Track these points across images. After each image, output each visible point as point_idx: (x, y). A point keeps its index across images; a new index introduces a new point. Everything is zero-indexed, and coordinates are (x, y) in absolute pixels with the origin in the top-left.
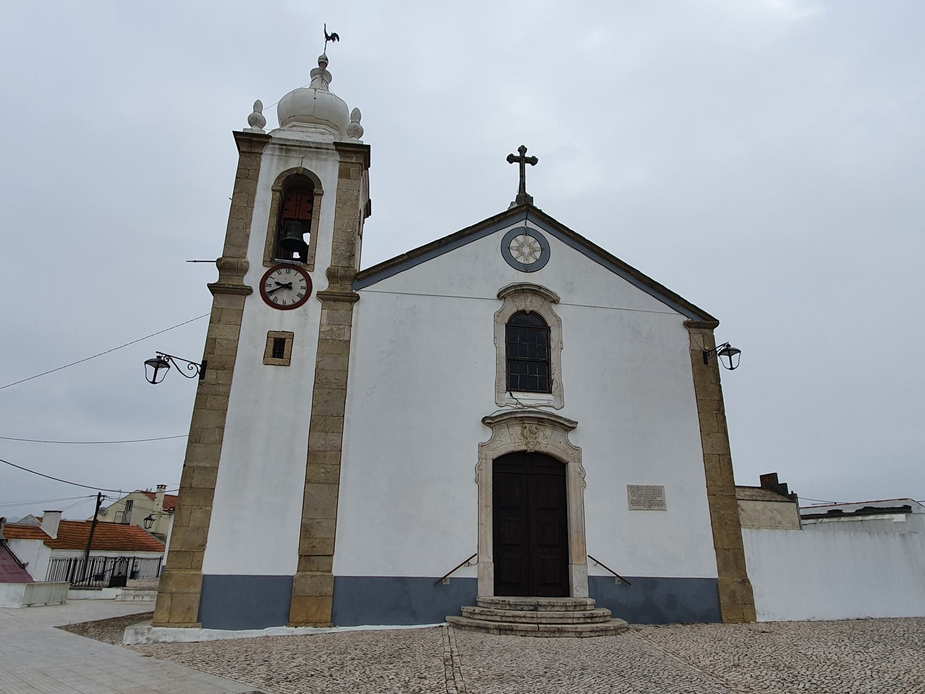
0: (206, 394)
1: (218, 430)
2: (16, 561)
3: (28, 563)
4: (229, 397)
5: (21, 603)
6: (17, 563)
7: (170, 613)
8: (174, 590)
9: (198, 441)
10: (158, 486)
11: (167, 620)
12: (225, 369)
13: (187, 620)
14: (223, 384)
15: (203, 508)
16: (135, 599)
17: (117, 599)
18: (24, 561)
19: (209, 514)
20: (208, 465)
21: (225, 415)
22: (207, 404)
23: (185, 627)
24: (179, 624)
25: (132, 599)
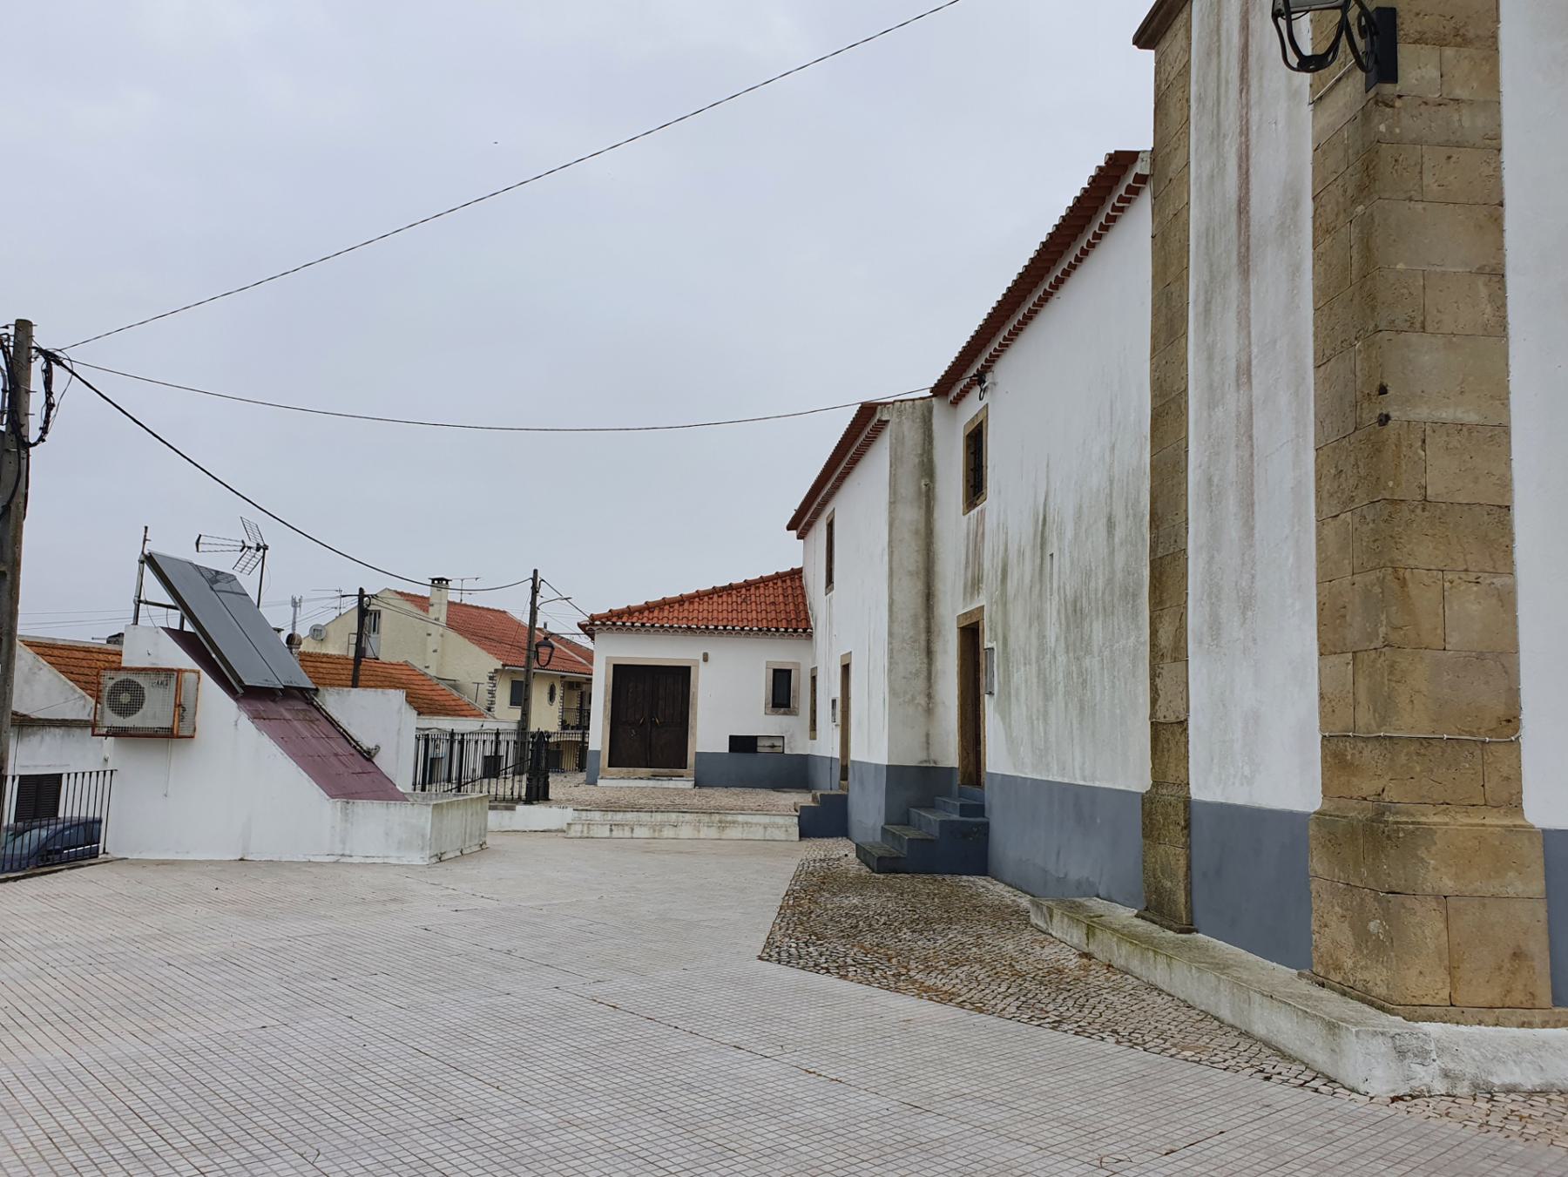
0: (1414, 142)
1: (1486, 285)
2: (350, 744)
3: (377, 748)
4: (1500, 150)
5: (428, 852)
6: (354, 747)
7: (1452, 970)
8: (1448, 884)
9: (1418, 325)
10: (433, 580)
11: (1445, 993)
12: (1466, 42)
13: (1518, 997)
14: (1472, 102)
15: (1486, 579)
16: (615, 834)
17: (572, 833)
18: (367, 743)
19: (1506, 600)
20: (1472, 418)
21: (1497, 221)
22: (1425, 182)
23: (1522, 1025)
24: (1495, 1012)
25: (607, 834)
